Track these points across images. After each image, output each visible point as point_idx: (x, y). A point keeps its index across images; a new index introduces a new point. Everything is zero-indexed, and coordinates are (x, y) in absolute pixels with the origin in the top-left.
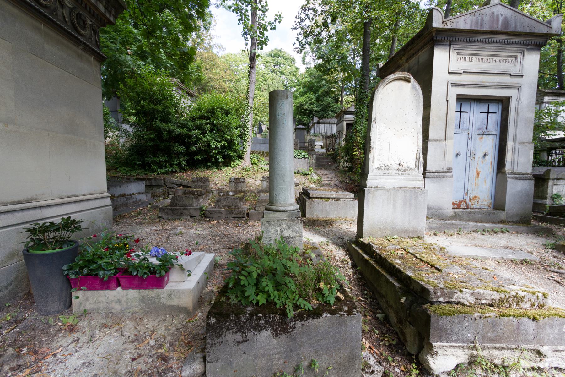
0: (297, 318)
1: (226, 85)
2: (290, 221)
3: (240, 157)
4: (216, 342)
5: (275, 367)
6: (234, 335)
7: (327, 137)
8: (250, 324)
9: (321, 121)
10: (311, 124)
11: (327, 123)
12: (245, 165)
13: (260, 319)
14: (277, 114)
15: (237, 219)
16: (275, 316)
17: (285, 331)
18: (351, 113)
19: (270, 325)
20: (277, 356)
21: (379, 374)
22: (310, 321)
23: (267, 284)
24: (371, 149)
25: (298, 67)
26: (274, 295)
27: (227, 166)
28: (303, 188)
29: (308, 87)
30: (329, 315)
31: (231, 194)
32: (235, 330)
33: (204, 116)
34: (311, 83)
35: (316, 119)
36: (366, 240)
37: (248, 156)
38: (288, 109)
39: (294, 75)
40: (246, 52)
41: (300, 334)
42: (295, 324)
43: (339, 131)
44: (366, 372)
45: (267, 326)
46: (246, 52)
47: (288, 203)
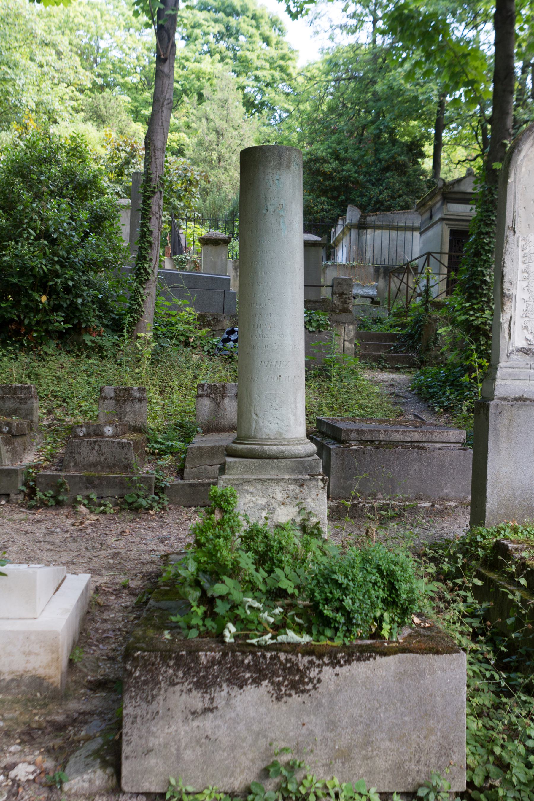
6: (184, 696)
9: (371, 219)
11: (390, 228)
31: (109, 430)
32: (187, 686)
43: (429, 254)
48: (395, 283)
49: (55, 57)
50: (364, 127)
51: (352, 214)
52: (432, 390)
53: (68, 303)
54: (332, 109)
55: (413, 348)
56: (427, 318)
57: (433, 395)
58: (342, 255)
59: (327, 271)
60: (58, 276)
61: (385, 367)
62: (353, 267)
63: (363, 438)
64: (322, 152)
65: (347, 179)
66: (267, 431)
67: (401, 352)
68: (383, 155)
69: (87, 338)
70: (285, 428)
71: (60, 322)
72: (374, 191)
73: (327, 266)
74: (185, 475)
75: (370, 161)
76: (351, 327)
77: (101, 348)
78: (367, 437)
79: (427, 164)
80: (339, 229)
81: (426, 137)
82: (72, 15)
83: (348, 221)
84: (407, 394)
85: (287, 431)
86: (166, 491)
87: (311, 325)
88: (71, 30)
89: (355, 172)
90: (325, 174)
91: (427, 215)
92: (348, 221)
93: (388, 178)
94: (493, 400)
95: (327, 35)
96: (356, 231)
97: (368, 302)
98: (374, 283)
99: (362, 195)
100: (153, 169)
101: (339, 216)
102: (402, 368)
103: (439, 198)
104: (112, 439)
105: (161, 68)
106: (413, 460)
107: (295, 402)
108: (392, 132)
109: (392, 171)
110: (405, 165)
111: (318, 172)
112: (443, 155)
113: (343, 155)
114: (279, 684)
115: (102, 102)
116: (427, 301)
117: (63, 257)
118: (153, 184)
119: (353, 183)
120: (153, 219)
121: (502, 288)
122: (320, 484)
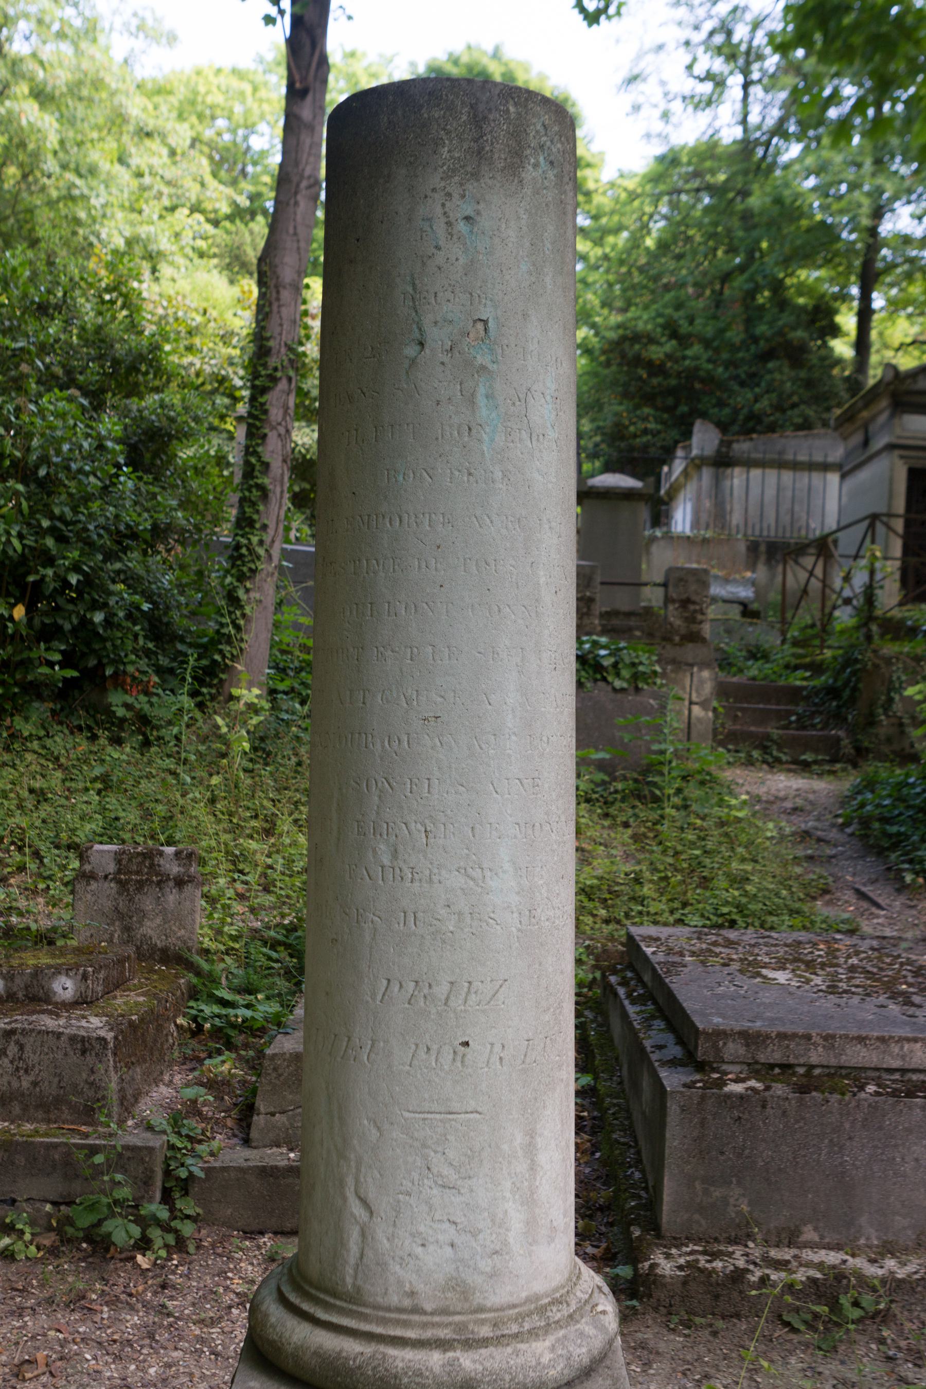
9: (742, 447)
11: (781, 465)
48: (795, 577)
49: (166, 159)
50: (726, 278)
51: (704, 438)
52: (894, 829)
53: (75, 621)
54: (663, 246)
55: (838, 718)
56: (869, 654)
57: (897, 841)
58: (682, 519)
59: (654, 549)
60: (50, 561)
61: (778, 760)
62: (705, 541)
63: (762, 1058)
64: (646, 322)
65: (692, 374)
66: (409, 1278)
67: (813, 726)
68: (762, 329)
69: (117, 700)
70: (485, 1265)
71: (51, 664)
72: (743, 397)
73: (653, 539)
74: (254, 1134)
75: (737, 340)
76: (706, 674)
77: (144, 720)
78: (773, 1054)
79: (843, 348)
80: (679, 466)
81: (844, 297)
82: (202, 89)
83: (695, 452)
84: (834, 834)
85: (494, 1275)
86: (195, 1189)
87: (618, 675)
88: (200, 117)
89: (709, 361)
90: (650, 365)
91: (858, 438)
92: (695, 452)
93: (770, 372)
95: (657, 113)
97: (735, 612)
98: (749, 574)
99: (721, 404)
100: (273, 328)
101: (676, 442)
102: (815, 762)
103: (884, 403)
105: (296, 109)
106: (909, 1131)
107: (530, 1149)
108: (778, 287)
109: (778, 358)
110: (802, 349)
111: (638, 361)
112: (874, 334)
113: (685, 328)
115: (248, 239)
116: (871, 618)
117: (62, 518)
118: (273, 361)
119: (702, 381)
120: (272, 437)
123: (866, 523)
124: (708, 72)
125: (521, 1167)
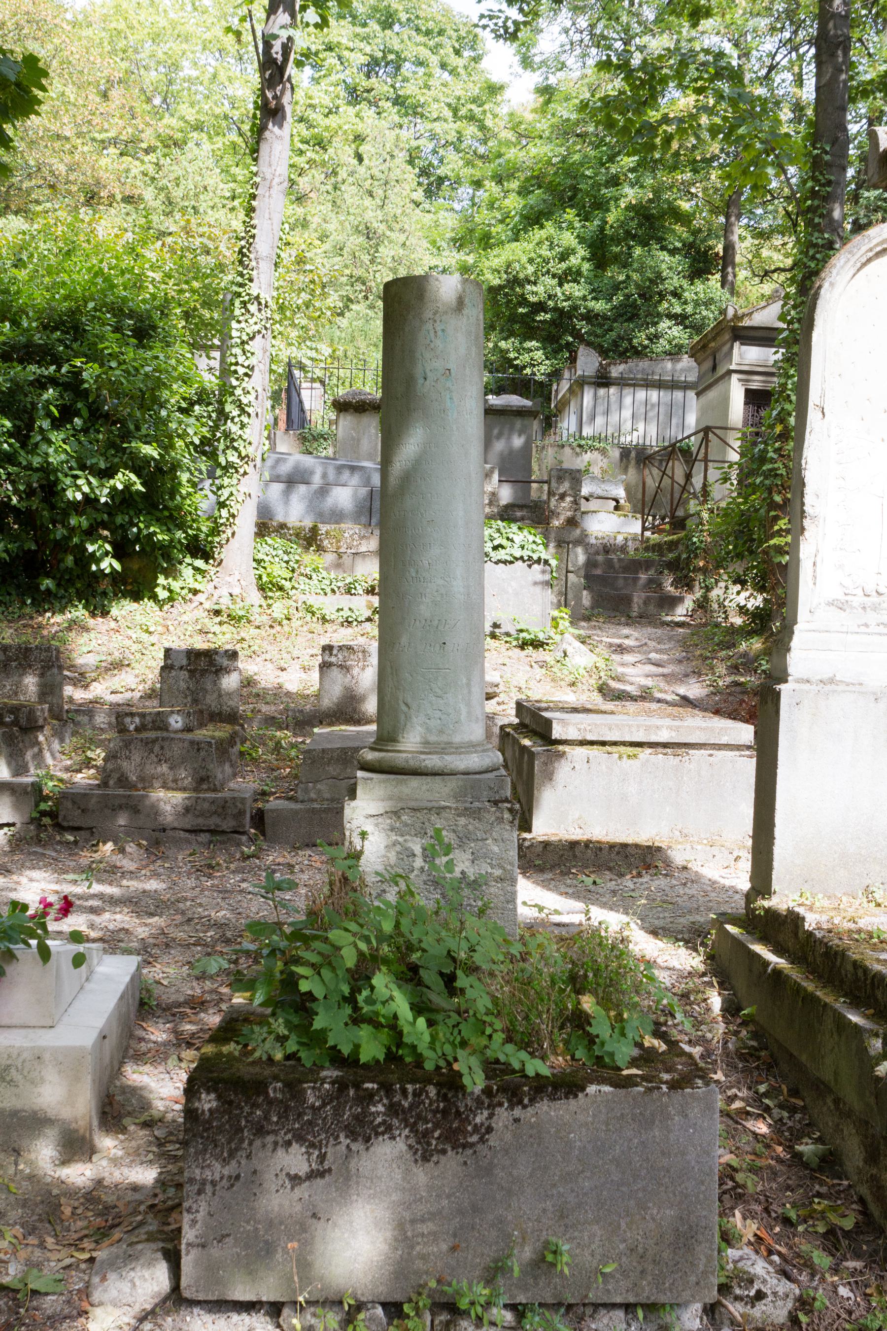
0: (500, 1097)
1: (108, 163)
2: (467, 812)
3: (200, 549)
4: (217, 1177)
5: (419, 1264)
7: (637, 457)
8: (338, 1112)
9: (616, 371)
10: (565, 386)
11: (648, 384)
12: (224, 591)
13: (370, 1096)
14: (418, 371)
15: (204, 837)
16: (422, 1090)
17: (455, 1139)
18: (762, 337)
19: (405, 1120)
20: (424, 1228)
21: (780, 1303)
22: (544, 1107)
23: (390, 995)
24: (806, 523)
25: (496, 78)
26: (418, 1030)
27: (137, 597)
28: (519, 705)
29: (551, 188)
30: (607, 1089)
31: (176, 722)
33: (29, 344)
34: (568, 170)
35: (588, 362)
36: (782, 899)
37: (239, 548)
38: (462, 351)
39: (471, 118)
40: (247, 37)
41: (507, 1152)
42: (491, 1116)
44: (738, 1298)
45: (395, 1122)
46: (247, 37)
47: (457, 739)
80: (565, 386)
91: (708, 364)
92: (579, 372)
94: (786, 681)
96: (592, 391)
104: (180, 735)
107: (468, 685)
114: (426, 1134)
121: (803, 504)
122: (507, 816)
123: (702, 434)
124: (426, 743)
125: (465, 691)
